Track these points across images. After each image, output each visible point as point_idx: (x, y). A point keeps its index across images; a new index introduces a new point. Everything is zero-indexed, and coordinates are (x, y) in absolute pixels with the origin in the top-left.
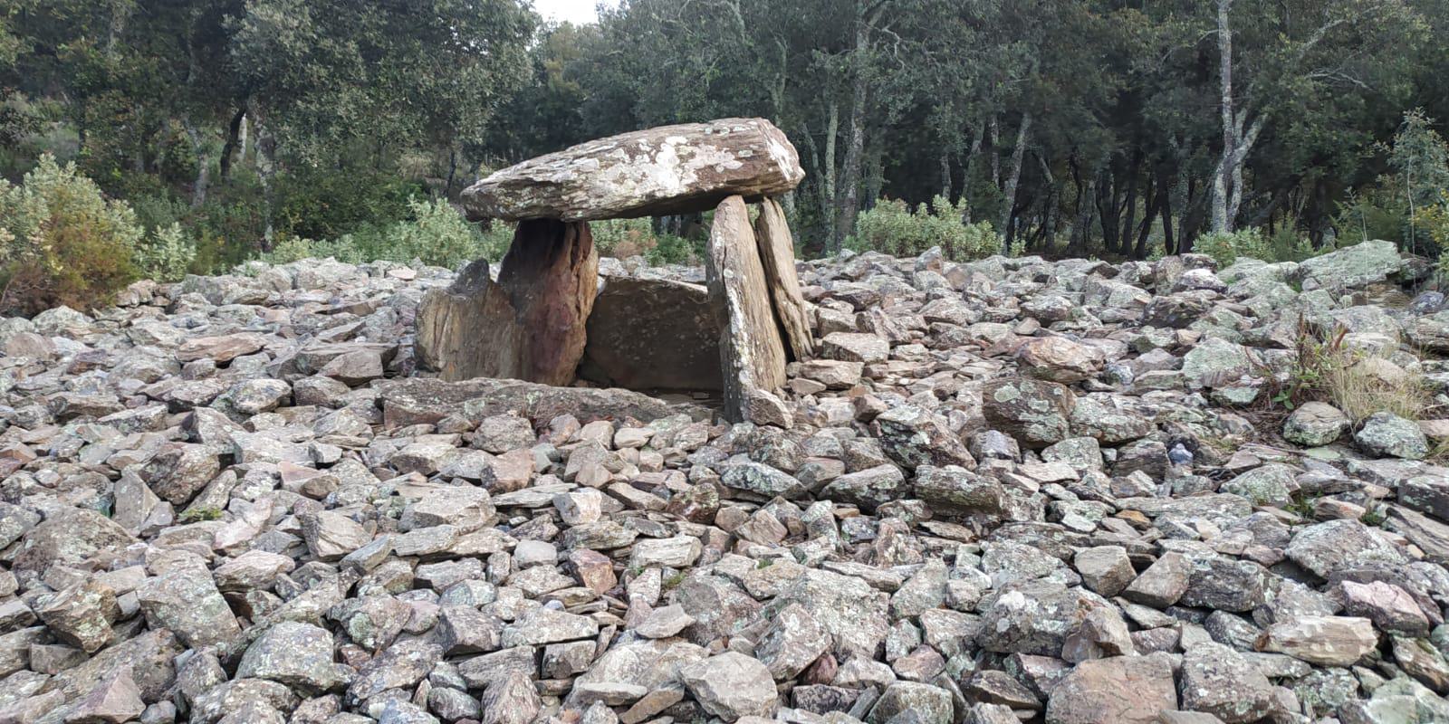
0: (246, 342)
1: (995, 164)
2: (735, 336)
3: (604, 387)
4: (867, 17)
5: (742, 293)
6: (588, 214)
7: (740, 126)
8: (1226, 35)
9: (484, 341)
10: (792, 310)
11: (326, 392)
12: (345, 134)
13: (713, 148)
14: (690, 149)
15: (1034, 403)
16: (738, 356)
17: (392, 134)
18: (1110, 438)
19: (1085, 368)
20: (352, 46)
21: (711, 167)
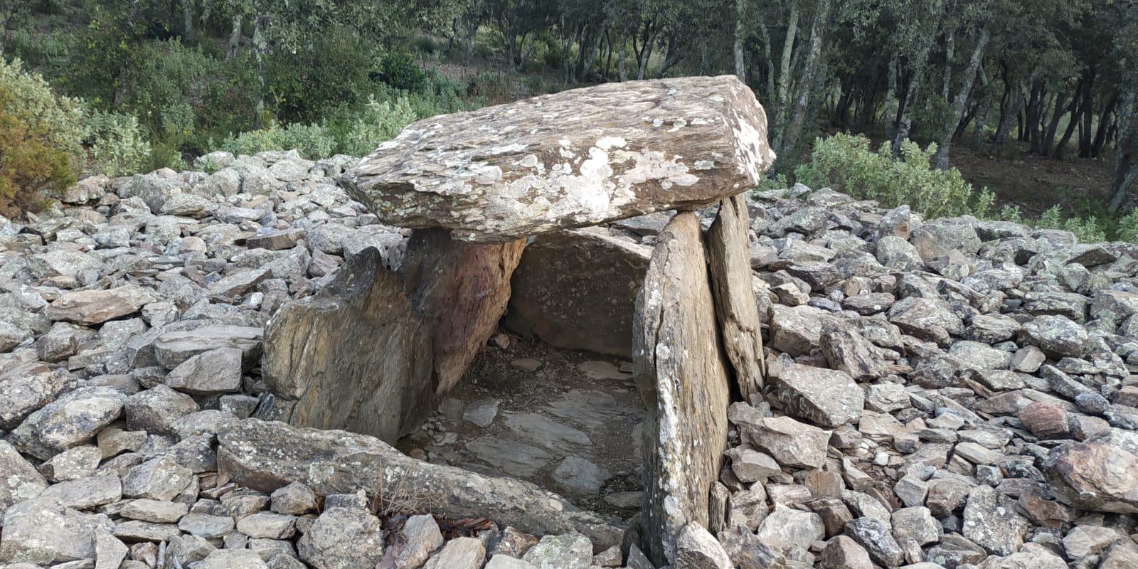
1: (947, 78)
2: (665, 447)
6: (482, 239)
9: (363, 353)
11: (162, 412)
12: (324, 21)
13: (660, 155)
14: (628, 155)
16: (666, 475)
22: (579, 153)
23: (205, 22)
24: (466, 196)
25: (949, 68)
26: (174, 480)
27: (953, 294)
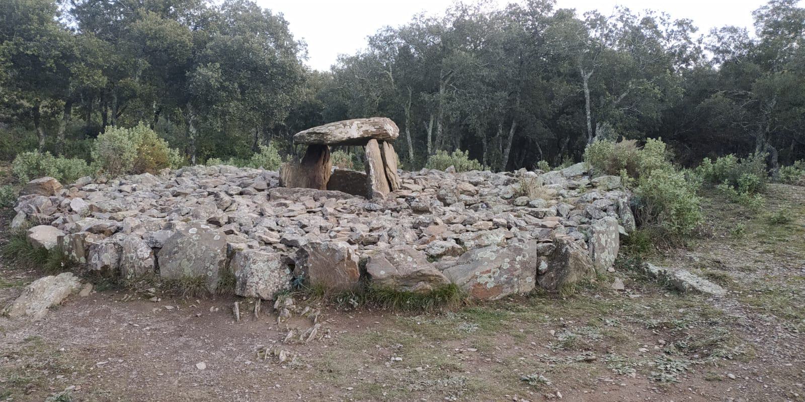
0: (221, 182)
3: (334, 190)
4: (444, 80)
5: (374, 164)
7: (376, 119)
8: (587, 91)
9: (298, 180)
10: (392, 175)
15: (449, 194)
17: (249, 120)
18: (468, 203)
19: (473, 191)
20: (236, 85)
21: (367, 130)
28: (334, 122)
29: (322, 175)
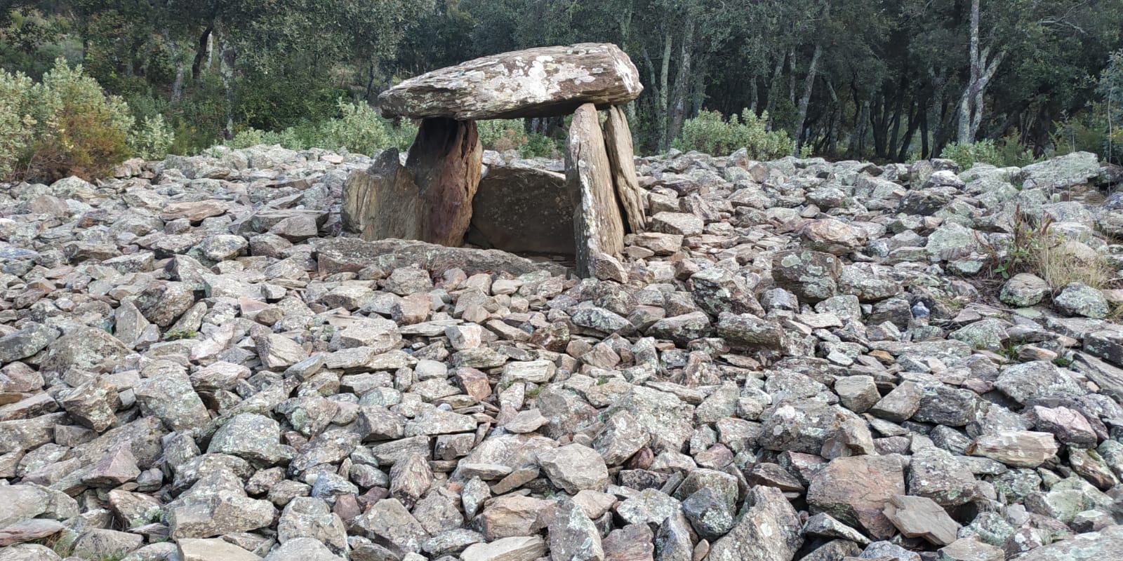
0: (213, 207)
1: (792, 85)
2: (586, 212)
7: (594, 49)
9: (395, 211)
10: (631, 194)
12: (289, 49)
14: (555, 66)
15: (811, 269)
16: (587, 227)
17: (325, 49)
18: (868, 296)
19: (852, 243)
21: (571, 80)
22: (527, 64)
23: (146, 71)
24: (465, 89)
25: (793, 78)
26: (296, 271)
27: (770, 189)
28: (483, 55)
29: (461, 182)
